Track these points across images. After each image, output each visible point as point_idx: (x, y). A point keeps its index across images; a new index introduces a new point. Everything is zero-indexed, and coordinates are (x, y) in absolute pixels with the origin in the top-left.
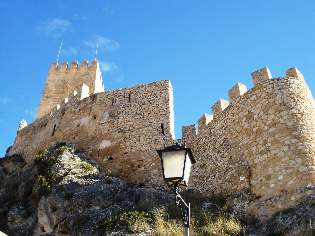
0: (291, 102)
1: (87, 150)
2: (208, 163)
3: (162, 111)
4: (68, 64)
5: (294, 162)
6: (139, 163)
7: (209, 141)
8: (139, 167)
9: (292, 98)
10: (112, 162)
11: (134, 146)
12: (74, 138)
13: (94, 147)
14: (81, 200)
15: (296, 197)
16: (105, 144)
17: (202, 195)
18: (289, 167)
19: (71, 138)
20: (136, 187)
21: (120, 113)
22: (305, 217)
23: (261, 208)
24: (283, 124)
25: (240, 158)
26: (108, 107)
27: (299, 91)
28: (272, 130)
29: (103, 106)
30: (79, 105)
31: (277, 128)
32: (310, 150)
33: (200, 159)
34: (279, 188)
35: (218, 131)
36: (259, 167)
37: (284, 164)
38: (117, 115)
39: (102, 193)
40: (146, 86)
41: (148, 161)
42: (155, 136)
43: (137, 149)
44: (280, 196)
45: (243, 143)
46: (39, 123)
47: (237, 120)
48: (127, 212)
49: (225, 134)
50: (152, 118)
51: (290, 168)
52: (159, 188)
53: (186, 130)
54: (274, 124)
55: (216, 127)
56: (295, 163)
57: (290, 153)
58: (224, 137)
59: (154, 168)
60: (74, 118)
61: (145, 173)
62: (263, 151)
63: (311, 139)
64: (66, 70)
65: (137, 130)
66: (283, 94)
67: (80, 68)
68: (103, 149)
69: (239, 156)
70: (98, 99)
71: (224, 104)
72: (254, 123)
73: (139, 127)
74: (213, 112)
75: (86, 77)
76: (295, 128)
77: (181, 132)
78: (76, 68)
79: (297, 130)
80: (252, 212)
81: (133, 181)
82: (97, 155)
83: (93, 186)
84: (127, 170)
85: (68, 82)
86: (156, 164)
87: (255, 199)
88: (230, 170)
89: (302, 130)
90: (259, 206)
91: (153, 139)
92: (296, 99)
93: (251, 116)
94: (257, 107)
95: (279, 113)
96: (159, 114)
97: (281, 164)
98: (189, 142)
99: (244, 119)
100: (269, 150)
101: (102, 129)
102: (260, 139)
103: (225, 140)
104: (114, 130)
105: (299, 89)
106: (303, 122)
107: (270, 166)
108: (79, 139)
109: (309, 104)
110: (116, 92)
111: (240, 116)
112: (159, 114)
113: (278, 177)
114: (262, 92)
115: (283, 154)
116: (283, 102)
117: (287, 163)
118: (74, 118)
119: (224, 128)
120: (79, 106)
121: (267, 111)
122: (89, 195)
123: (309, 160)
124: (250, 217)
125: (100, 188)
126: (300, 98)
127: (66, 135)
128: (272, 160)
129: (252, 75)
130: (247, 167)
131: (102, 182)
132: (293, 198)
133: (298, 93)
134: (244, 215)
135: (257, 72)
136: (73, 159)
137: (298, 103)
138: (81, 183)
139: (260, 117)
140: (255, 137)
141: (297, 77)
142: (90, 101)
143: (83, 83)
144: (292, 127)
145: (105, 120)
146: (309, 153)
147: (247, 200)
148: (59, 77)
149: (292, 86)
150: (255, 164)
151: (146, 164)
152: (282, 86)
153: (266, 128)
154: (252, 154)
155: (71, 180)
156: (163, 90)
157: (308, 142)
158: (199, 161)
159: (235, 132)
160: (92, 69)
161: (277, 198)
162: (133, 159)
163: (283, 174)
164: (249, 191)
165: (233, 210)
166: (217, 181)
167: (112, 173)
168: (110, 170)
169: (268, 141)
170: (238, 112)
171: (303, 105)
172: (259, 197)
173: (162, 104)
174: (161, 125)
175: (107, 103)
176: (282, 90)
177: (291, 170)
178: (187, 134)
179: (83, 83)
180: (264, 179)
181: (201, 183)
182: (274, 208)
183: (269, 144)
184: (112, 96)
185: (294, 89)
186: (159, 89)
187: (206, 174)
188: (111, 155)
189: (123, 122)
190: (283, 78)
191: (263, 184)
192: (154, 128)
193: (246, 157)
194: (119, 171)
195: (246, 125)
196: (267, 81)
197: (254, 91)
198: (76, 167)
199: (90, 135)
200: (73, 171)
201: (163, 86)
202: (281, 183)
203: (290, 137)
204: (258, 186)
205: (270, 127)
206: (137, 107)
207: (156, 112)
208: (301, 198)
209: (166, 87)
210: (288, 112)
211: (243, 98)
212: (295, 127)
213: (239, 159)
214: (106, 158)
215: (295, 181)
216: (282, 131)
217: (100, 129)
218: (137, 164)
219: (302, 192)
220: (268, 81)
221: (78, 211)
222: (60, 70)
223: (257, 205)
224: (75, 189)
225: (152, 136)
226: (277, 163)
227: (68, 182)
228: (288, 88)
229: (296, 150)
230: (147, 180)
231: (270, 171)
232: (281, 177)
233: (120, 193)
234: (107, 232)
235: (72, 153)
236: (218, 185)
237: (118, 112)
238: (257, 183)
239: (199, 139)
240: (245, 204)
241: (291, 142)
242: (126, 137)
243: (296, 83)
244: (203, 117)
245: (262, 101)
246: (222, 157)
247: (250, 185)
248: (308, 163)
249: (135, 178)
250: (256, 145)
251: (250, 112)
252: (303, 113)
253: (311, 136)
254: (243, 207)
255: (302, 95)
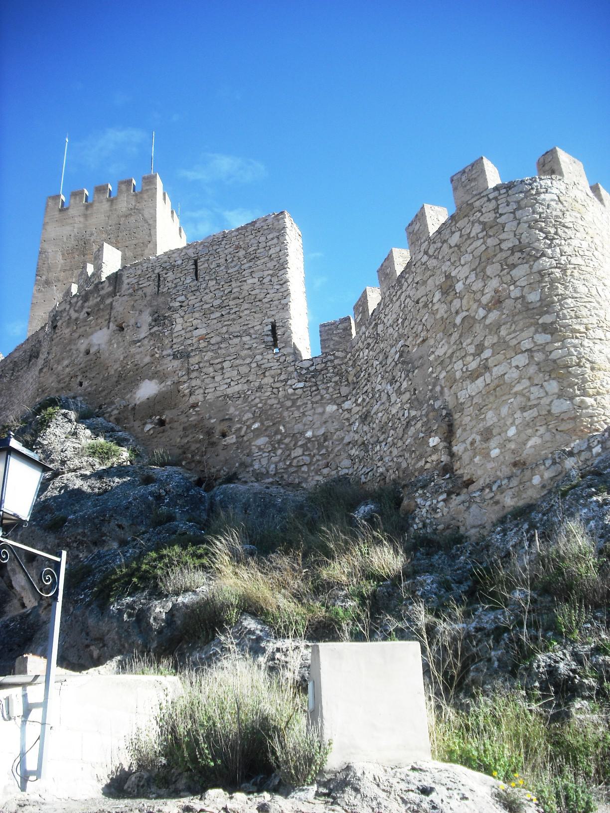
0: (539, 240)
1: (109, 410)
2: (376, 407)
3: (271, 291)
4: (86, 192)
5: (541, 390)
6: (223, 427)
7: (375, 354)
8: (224, 435)
9: (541, 230)
10: (164, 431)
11: (211, 386)
12: (81, 384)
13: (123, 399)
14: (80, 531)
15: (542, 477)
16: (147, 390)
17: (365, 486)
18: (530, 404)
19: (74, 384)
20: (221, 484)
21: (175, 311)
22: (544, 525)
23: (471, 510)
24: (516, 299)
25: (431, 391)
26: (148, 298)
27: (561, 210)
28: (494, 316)
29: (137, 298)
30: (85, 302)
31: (505, 311)
32: (578, 358)
33: (360, 400)
34: (509, 458)
35: (391, 330)
36: (469, 410)
37: (519, 399)
38: (169, 316)
39: (128, 508)
40: (233, 234)
41: (244, 419)
42: (259, 357)
43: (218, 393)
44: (509, 478)
45: (436, 353)
46: (25, 352)
47: (424, 299)
48: (157, 551)
49: (401, 336)
50: (248, 312)
51: (531, 408)
52: (271, 480)
53: (330, 332)
54: (498, 302)
55: (386, 321)
56: (542, 395)
57: (532, 369)
58: (401, 343)
59: (258, 433)
60: (76, 335)
61: (238, 448)
62: (475, 370)
63: (584, 330)
64: (83, 208)
65: (216, 347)
66: (519, 224)
67: (116, 198)
68: (142, 403)
69: (430, 387)
70: (126, 281)
71: (401, 258)
72: (457, 303)
73: (219, 339)
74: (381, 282)
75: (132, 219)
76: (546, 306)
77: (319, 339)
78: (108, 200)
79: (550, 310)
80: (454, 519)
81: (213, 470)
82: (131, 417)
83: (114, 494)
84: (198, 445)
85: (92, 239)
86: (262, 424)
87: (460, 488)
88: (413, 423)
89: (562, 309)
90: (467, 504)
91: (254, 365)
92: (552, 231)
93: (451, 286)
94: (463, 262)
95: (508, 273)
96: (266, 300)
97: (512, 400)
98: (336, 362)
99: (438, 296)
100: (487, 368)
101: (138, 353)
102: (469, 341)
103: (403, 351)
104: (165, 353)
105: (562, 203)
106: (566, 288)
107: (489, 406)
108: (91, 386)
109: (588, 238)
110: (166, 259)
111: (428, 289)
112: (266, 300)
113: (506, 432)
114: (473, 223)
115: (515, 374)
116: (520, 242)
117: (524, 395)
118: (76, 335)
119: (400, 321)
120: (86, 304)
121: (484, 270)
122: (97, 517)
123: (577, 383)
124: (449, 531)
125: (126, 497)
126: (564, 226)
127: (63, 379)
128: (495, 390)
129: (452, 181)
130: (444, 412)
131: (133, 482)
132: (536, 480)
133: (557, 216)
134: (436, 529)
135: (464, 172)
136: (75, 434)
137: (557, 241)
138: (89, 490)
139: (468, 287)
140: (460, 337)
141: (561, 174)
142: (108, 289)
143: (105, 245)
144: (538, 304)
145: (144, 332)
146: (578, 365)
147: (442, 493)
148: (68, 228)
149: (544, 200)
150: (462, 404)
151: (239, 426)
152: (518, 202)
153: (482, 312)
154: (455, 380)
155: (66, 487)
156: (273, 239)
157: (577, 338)
158: (359, 405)
159: (420, 328)
160: (145, 196)
161: (503, 483)
162: (210, 418)
163: (517, 422)
164: (447, 469)
165: (414, 519)
166: (391, 452)
167: (162, 456)
168: (159, 451)
169: (486, 344)
170: (425, 279)
171: (569, 244)
172: (470, 482)
173: (272, 276)
174: (270, 327)
175: (145, 290)
176: (519, 214)
177: (533, 413)
178: (332, 342)
179: (105, 245)
180: (478, 438)
181: (363, 458)
182: (496, 508)
183: (487, 353)
184: (156, 272)
185: (548, 206)
186: (263, 239)
187: (371, 437)
188: (161, 414)
189: (183, 332)
190: (522, 181)
191: (477, 450)
192: (253, 336)
193: (442, 388)
194: (181, 451)
195: (442, 310)
196: (483, 193)
197: (456, 223)
198: (79, 453)
199: (112, 372)
200: (71, 465)
201: (270, 229)
202: (512, 446)
203: (533, 329)
204: (466, 457)
205: (489, 311)
206: (212, 289)
207: (259, 297)
208: (552, 479)
209: (279, 230)
210: (531, 267)
211: (434, 243)
212: (545, 303)
213: (429, 394)
214: (151, 423)
215: (541, 436)
216: (516, 318)
217: (133, 356)
218: (219, 429)
219: (554, 463)
220: (484, 193)
221: (78, 556)
222: (71, 212)
223: (463, 502)
224: (73, 505)
225: (249, 356)
226: (504, 398)
227: (60, 491)
228: (532, 206)
229: (546, 360)
230: (243, 465)
231: (490, 417)
232: (512, 432)
233: (168, 505)
234: (112, 600)
235: (70, 421)
236: (392, 460)
237: (170, 308)
238: (466, 450)
239: (357, 351)
240: (438, 502)
241: (535, 342)
242: (192, 368)
243: (554, 191)
244: (362, 296)
245: (472, 247)
246: (399, 393)
247: (452, 455)
248: (574, 390)
249: (216, 464)
250: (462, 358)
251: (448, 277)
252: (568, 266)
253: (585, 321)
254: (435, 510)
255: (567, 220)
